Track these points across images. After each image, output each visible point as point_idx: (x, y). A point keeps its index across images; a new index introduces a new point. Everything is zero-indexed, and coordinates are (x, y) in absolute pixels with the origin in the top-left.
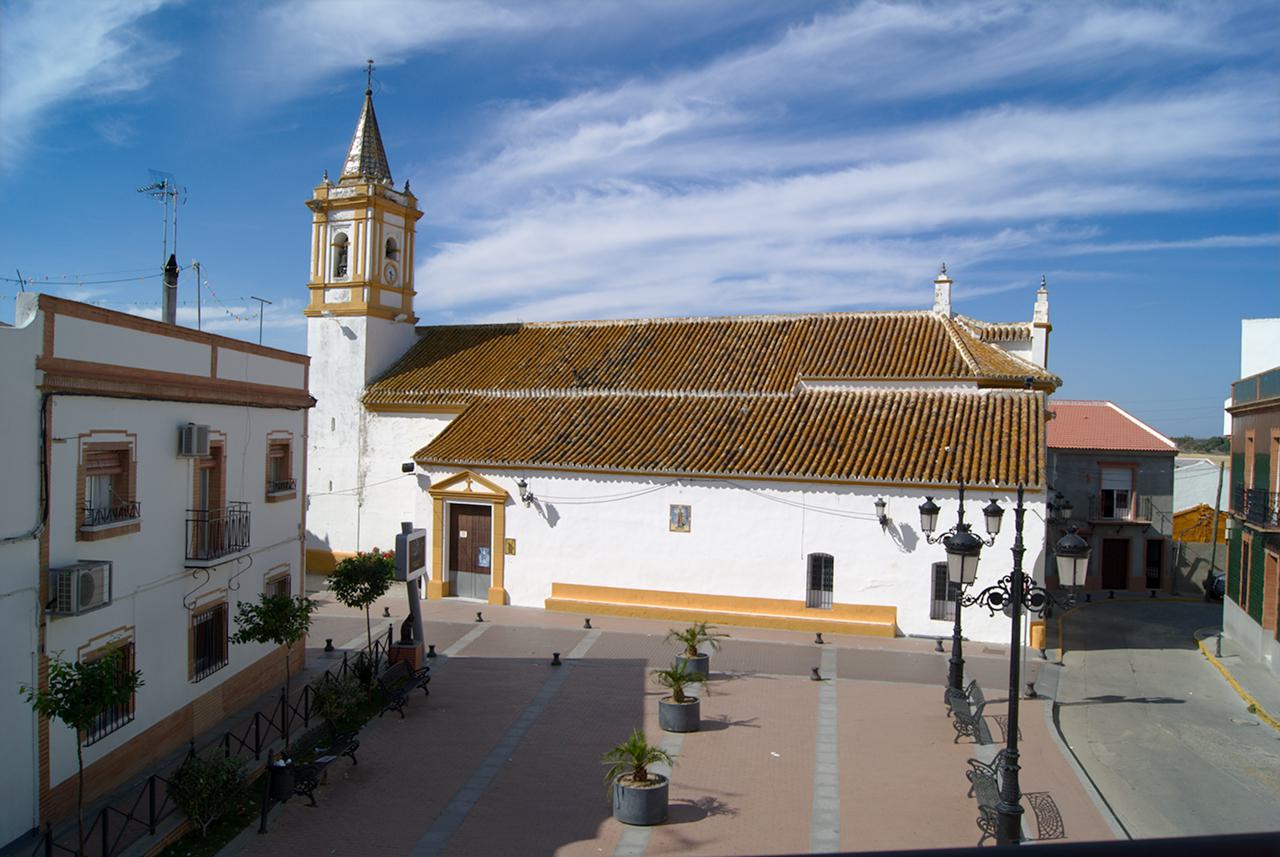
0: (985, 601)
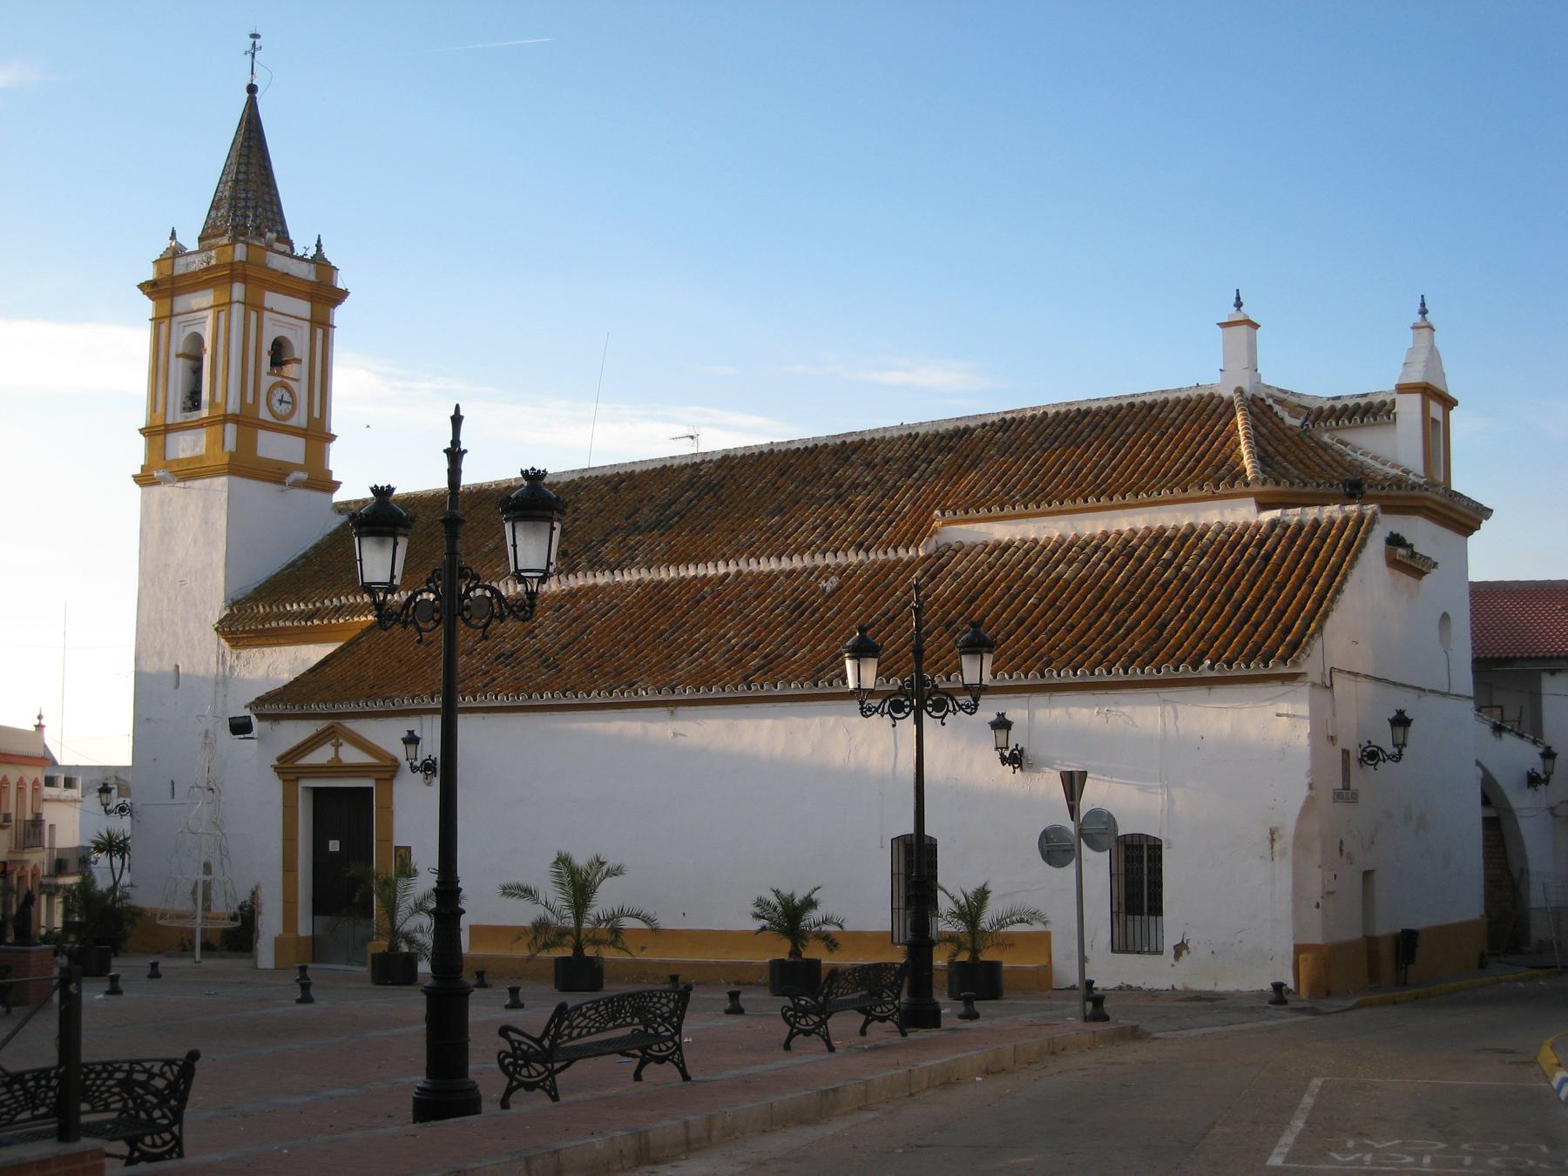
0: (886, 710)
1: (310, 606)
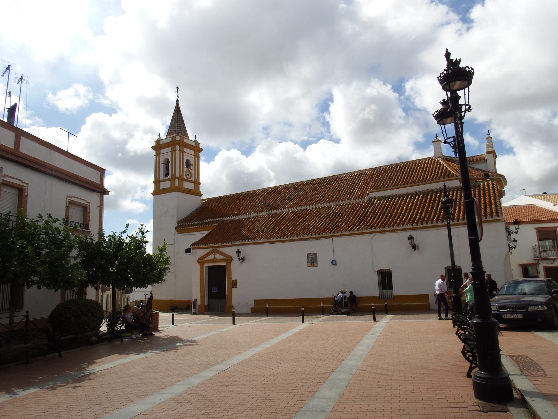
1: (200, 222)
